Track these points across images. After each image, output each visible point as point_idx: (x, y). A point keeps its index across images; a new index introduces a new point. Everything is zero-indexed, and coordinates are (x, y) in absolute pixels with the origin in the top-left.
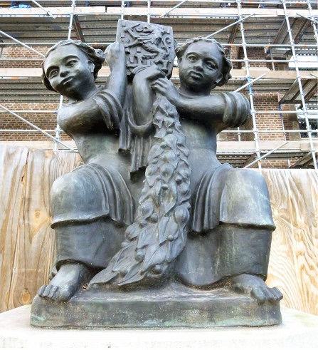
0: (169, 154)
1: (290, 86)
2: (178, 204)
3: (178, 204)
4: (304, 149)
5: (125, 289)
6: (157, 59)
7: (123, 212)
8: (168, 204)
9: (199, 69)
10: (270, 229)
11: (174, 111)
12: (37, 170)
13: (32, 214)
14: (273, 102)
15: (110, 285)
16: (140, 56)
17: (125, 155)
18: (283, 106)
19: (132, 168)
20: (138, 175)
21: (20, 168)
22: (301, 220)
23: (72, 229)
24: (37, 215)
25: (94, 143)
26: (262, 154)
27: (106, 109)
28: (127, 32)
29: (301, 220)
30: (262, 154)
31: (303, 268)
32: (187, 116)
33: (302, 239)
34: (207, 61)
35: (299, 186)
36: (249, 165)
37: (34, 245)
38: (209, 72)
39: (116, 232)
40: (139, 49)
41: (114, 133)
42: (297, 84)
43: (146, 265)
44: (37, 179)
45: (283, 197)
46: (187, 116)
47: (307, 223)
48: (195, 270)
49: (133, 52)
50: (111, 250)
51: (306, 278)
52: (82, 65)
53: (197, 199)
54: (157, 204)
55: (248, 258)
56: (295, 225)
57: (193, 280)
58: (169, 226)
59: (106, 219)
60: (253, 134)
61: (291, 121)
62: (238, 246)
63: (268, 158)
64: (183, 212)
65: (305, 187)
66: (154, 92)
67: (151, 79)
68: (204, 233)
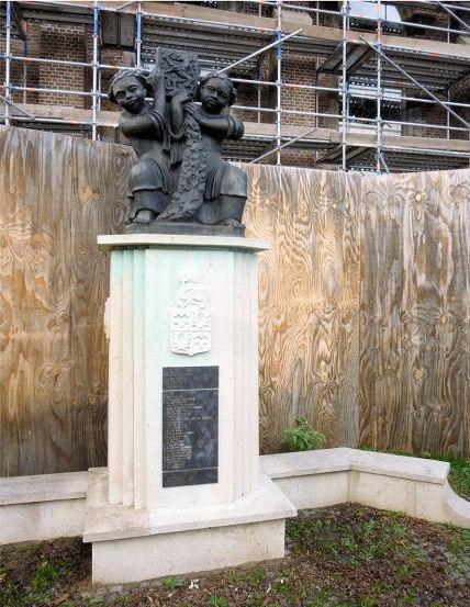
0: (195, 156)
1: (332, 49)
2: (200, 183)
3: (200, 183)
4: (334, 140)
5: (174, 220)
6: (187, 84)
7: (168, 187)
8: (194, 183)
9: (215, 98)
10: (245, 198)
11: (198, 128)
12: (81, 156)
13: (80, 191)
14: (307, 70)
15: (163, 219)
16: (174, 80)
17: (167, 153)
18: (322, 76)
19: (172, 162)
20: (176, 166)
21: (68, 154)
22: (286, 208)
23: (145, 193)
24: (84, 192)
25: (145, 143)
26: (283, 142)
27: (156, 123)
28: (165, 59)
29: (286, 208)
30: (283, 142)
31: (282, 243)
32: (206, 130)
33: (285, 223)
34: (220, 93)
35: (289, 180)
36: (430, 101)
37: (84, 214)
38: (221, 101)
39: (165, 198)
40: (174, 75)
41: (160, 140)
42: (341, 48)
43: (184, 210)
44: (81, 163)
45: (275, 189)
46: (206, 130)
47: (290, 211)
48: (206, 216)
49: (169, 76)
50: (164, 206)
51: (284, 251)
52: (140, 92)
53: (209, 181)
54: (189, 183)
55: (233, 211)
56: (282, 212)
57: (205, 221)
58: (195, 194)
59: (160, 189)
60: (275, 114)
61: (328, 101)
62: (229, 206)
63: (291, 147)
64: (202, 187)
65: (293, 182)
66: (185, 112)
67: (183, 103)
68: (212, 200)
